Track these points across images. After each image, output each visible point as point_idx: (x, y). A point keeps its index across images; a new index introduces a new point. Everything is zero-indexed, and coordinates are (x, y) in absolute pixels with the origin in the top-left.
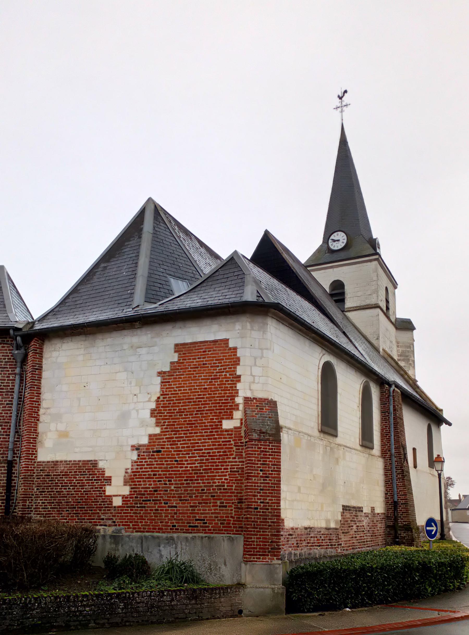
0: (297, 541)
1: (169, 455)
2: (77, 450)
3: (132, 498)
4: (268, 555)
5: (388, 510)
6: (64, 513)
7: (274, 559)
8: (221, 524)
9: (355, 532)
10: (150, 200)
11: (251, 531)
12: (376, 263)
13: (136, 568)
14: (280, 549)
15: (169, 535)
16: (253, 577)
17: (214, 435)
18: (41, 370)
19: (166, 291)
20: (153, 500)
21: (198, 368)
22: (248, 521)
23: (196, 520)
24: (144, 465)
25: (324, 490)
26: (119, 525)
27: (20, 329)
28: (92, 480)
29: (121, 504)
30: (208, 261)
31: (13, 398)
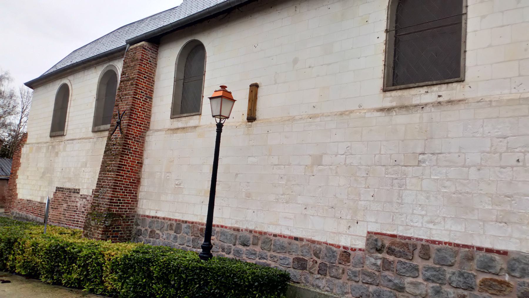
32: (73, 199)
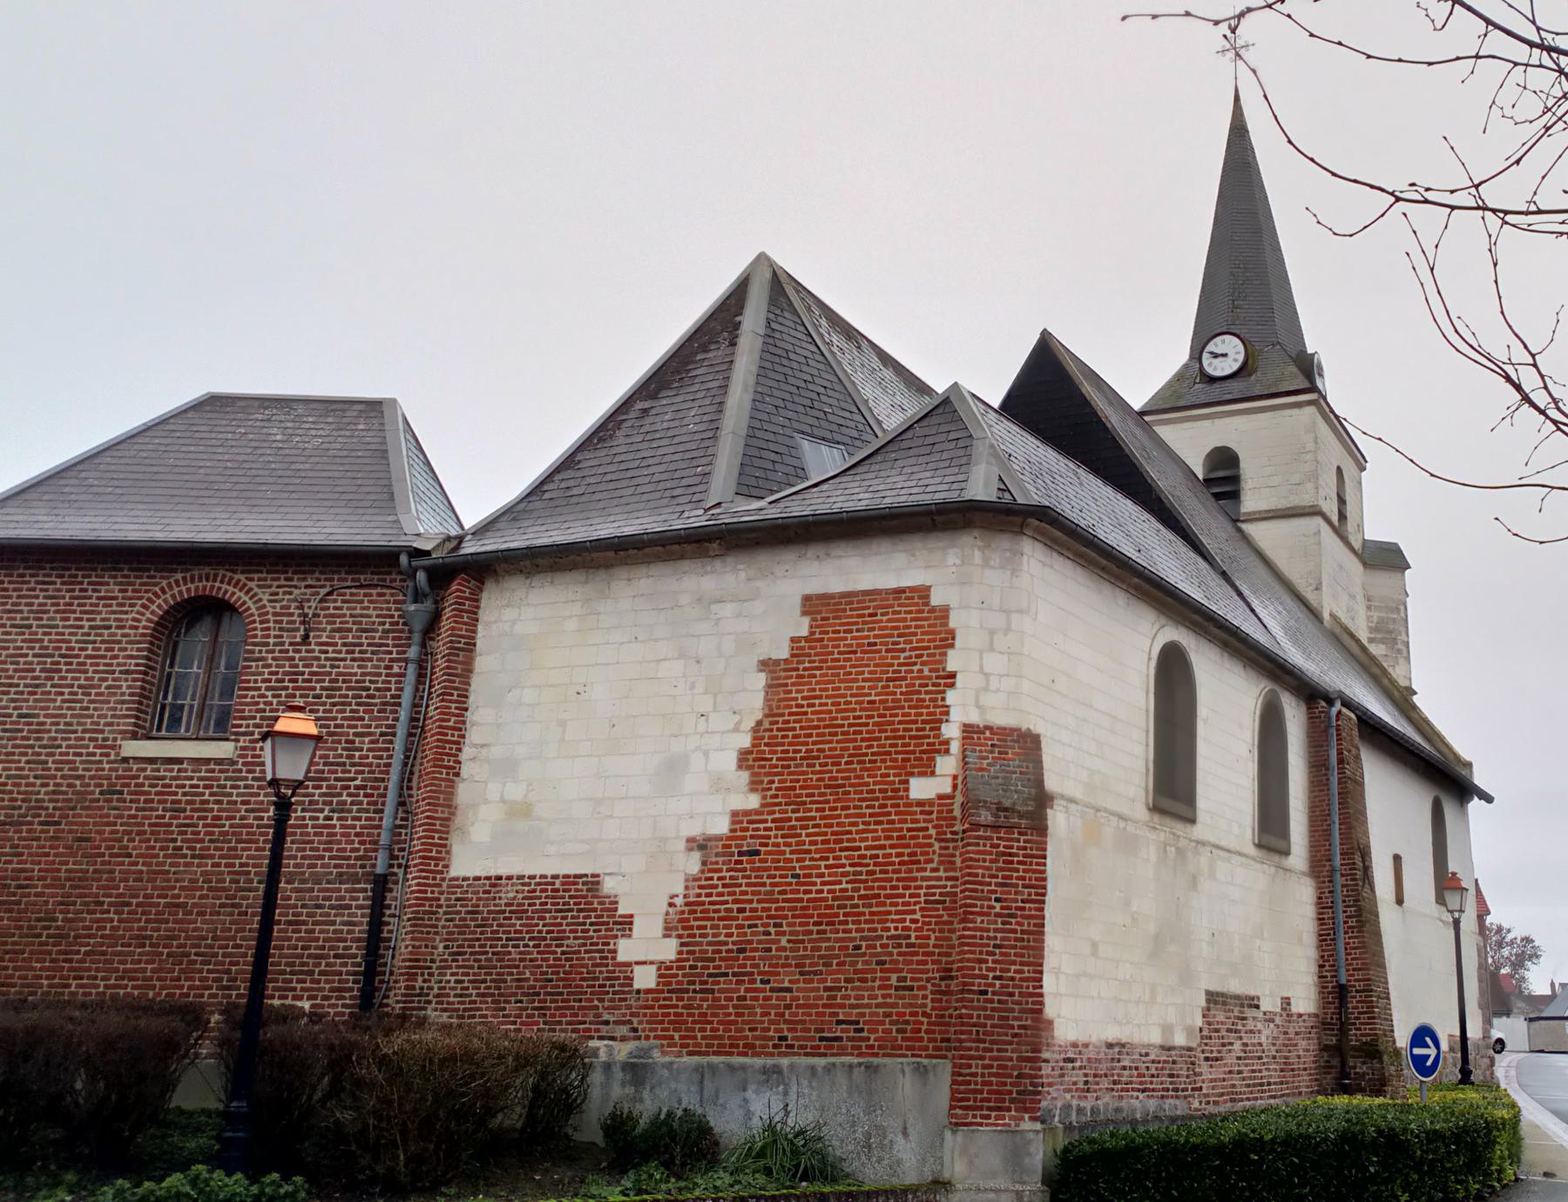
0: (1086, 1075)
1: (778, 861)
2: (552, 849)
3: (683, 968)
4: (1009, 1110)
5: (1324, 1001)
6: (511, 1009)
7: (1022, 1119)
8: (898, 1031)
9: (1239, 1058)
10: (762, 258)
11: (970, 1049)
12: (1312, 410)
13: (684, 1145)
14: (1039, 1093)
15: (770, 1061)
16: (971, 1163)
17: (889, 814)
18: (471, 651)
19: (791, 470)
20: (734, 974)
21: (855, 652)
22: (963, 1024)
23: (839, 1022)
24: (716, 887)
25: (1159, 953)
26: (647, 1038)
27: (427, 553)
28: (584, 924)
29: (653, 985)
30: (898, 399)
31: (396, 719)
32: (1250, 1025)
